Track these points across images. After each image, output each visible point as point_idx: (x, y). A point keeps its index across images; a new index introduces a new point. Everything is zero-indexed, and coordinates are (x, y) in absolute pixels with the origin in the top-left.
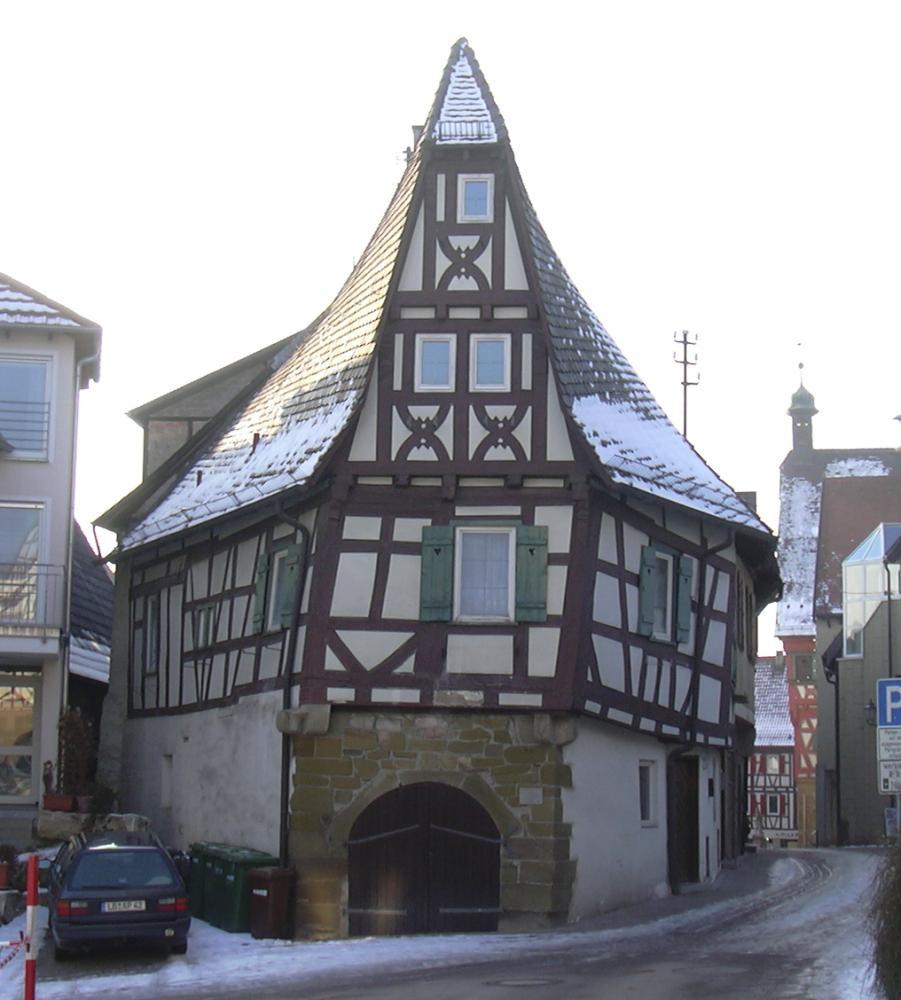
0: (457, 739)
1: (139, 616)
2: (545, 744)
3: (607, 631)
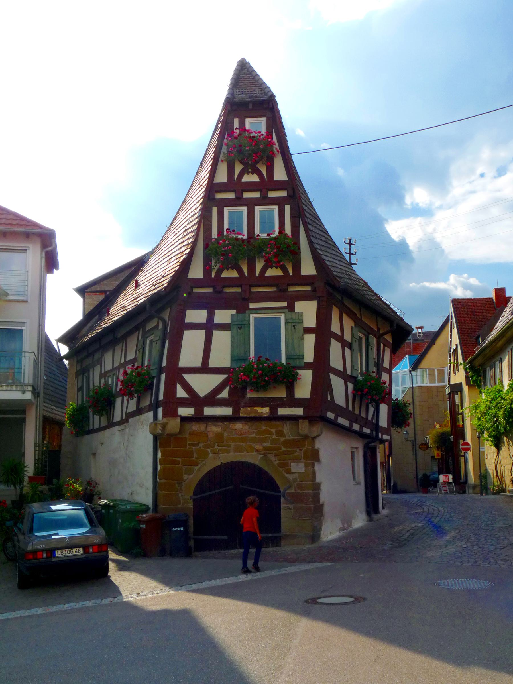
0: (254, 435)
1: (80, 385)
2: (306, 437)
3: (337, 373)
